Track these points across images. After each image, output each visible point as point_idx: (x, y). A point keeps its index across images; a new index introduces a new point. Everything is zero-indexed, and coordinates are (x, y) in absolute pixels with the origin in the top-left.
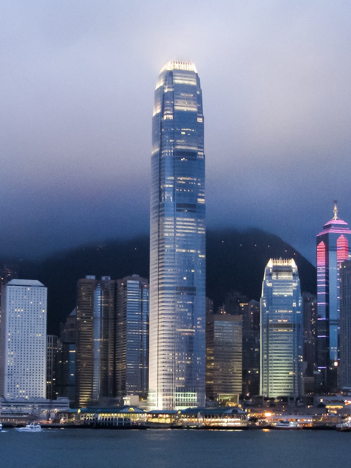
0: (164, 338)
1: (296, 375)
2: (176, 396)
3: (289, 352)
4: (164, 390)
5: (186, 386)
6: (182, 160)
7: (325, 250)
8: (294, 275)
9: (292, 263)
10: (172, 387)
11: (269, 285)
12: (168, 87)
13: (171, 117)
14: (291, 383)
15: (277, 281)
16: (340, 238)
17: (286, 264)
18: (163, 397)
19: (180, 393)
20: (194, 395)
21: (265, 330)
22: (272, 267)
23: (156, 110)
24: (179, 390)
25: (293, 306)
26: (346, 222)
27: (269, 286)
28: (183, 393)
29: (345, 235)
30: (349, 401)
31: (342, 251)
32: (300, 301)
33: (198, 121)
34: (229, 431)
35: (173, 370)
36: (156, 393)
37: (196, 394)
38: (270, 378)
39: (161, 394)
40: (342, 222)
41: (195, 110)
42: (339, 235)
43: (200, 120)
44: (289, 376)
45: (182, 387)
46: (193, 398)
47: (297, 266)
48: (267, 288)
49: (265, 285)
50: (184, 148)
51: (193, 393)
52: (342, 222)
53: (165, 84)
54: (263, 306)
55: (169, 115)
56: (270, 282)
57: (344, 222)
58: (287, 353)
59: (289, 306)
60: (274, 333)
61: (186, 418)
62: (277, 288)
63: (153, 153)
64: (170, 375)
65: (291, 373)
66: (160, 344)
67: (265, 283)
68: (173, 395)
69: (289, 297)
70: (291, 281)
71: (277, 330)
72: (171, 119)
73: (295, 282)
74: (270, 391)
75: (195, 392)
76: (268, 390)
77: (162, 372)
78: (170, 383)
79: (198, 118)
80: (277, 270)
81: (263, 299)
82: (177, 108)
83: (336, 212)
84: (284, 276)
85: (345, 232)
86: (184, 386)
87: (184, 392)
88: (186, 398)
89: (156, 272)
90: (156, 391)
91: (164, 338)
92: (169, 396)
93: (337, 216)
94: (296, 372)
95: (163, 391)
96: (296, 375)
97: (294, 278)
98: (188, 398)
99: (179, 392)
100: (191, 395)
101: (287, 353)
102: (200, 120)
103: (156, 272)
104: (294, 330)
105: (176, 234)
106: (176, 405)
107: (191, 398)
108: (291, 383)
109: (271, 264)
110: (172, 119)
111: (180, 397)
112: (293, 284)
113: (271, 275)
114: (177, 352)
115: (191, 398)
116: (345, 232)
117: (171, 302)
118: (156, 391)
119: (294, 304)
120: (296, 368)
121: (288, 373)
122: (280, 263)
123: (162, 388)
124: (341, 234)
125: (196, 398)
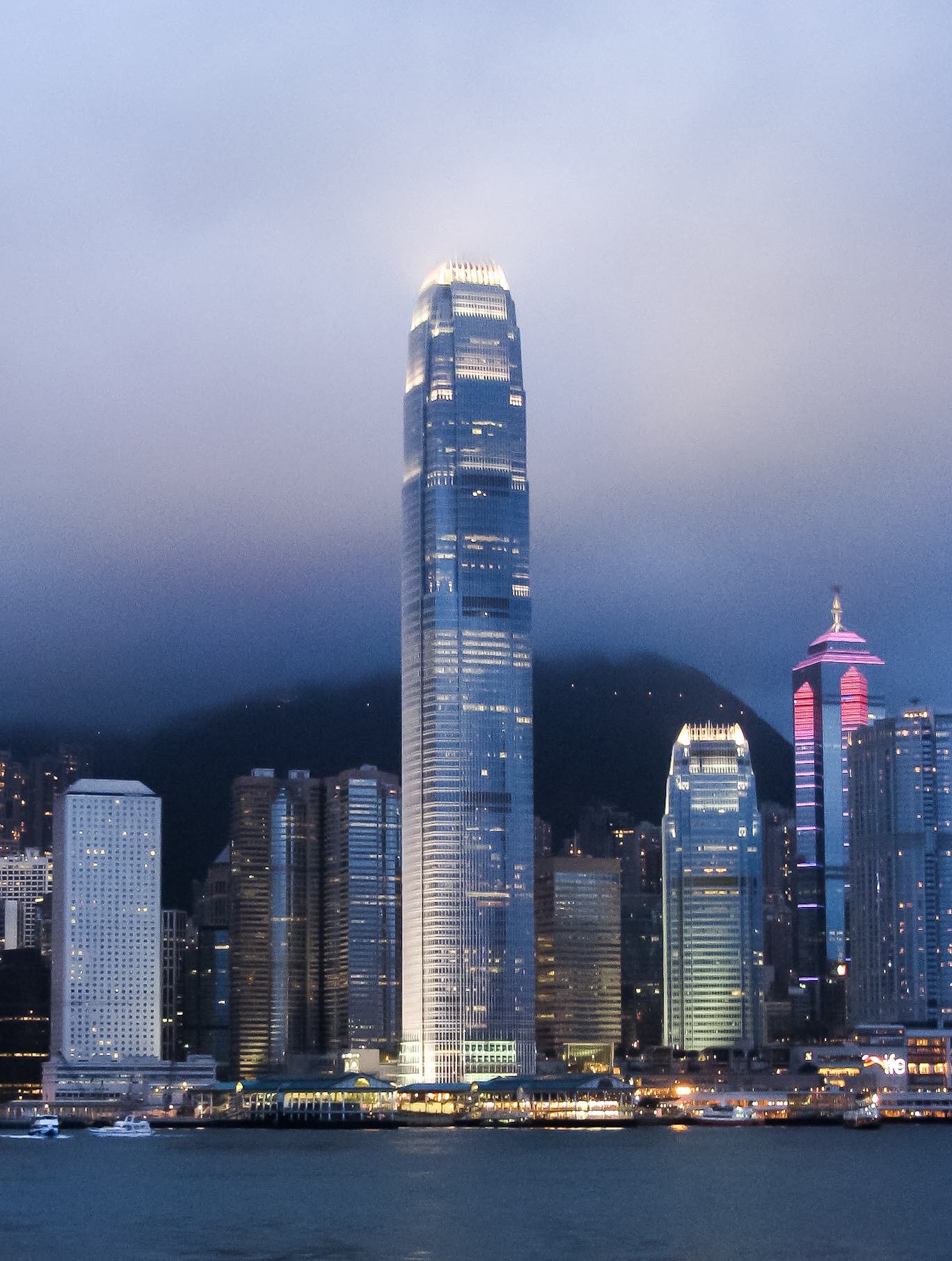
0: (436, 914)
1: (748, 998)
4: (438, 1037)
8: (740, 762)
10: (456, 1029)
13: (447, 394)
14: (735, 1016)
15: (701, 776)
17: (721, 737)
18: (437, 1052)
19: (477, 1043)
21: (674, 893)
23: (412, 379)
24: (473, 1035)
26: (860, 636)
28: (483, 1043)
30: (872, 1058)
31: (852, 704)
32: (755, 823)
35: (458, 990)
36: (419, 1044)
39: (430, 1044)
40: (851, 637)
41: (503, 376)
43: (517, 399)
46: (507, 1053)
47: (747, 742)
49: (674, 788)
51: (507, 1043)
52: (851, 637)
53: (434, 317)
54: (669, 835)
56: (684, 780)
57: (856, 636)
61: (491, 1100)
62: (702, 794)
65: (736, 993)
66: (427, 929)
67: (673, 781)
68: (458, 1046)
69: (730, 814)
70: (734, 778)
73: (743, 779)
74: (686, 1035)
75: (510, 1039)
80: (702, 751)
81: (669, 819)
82: (461, 373)
84: (719, 766)
85: (859, 660)
86: (484, 1026)
87: (486, 1039)
88: (489, 1054)
90: (419, 1038)
93: (841, 622)
94: (748, 989)
96: (748, 998)
97: (741, 770)
98: (495, 1053)
100: (501, 1048)
101: (726, 946)
102: (515, 401)
104: (742, 892)
107: (501, 1054)
108: (735, 1016)
109: (685, 737)
112: (739, 783)
113: (686, 762)
115: (501, 1054)
116: (859, 660)
117: (453, 829)
118: (420, 1038)
119: (742, 831)
120: (747, 982)
122: (708, 734)
123: (434, 1030)
124: (849, 665)
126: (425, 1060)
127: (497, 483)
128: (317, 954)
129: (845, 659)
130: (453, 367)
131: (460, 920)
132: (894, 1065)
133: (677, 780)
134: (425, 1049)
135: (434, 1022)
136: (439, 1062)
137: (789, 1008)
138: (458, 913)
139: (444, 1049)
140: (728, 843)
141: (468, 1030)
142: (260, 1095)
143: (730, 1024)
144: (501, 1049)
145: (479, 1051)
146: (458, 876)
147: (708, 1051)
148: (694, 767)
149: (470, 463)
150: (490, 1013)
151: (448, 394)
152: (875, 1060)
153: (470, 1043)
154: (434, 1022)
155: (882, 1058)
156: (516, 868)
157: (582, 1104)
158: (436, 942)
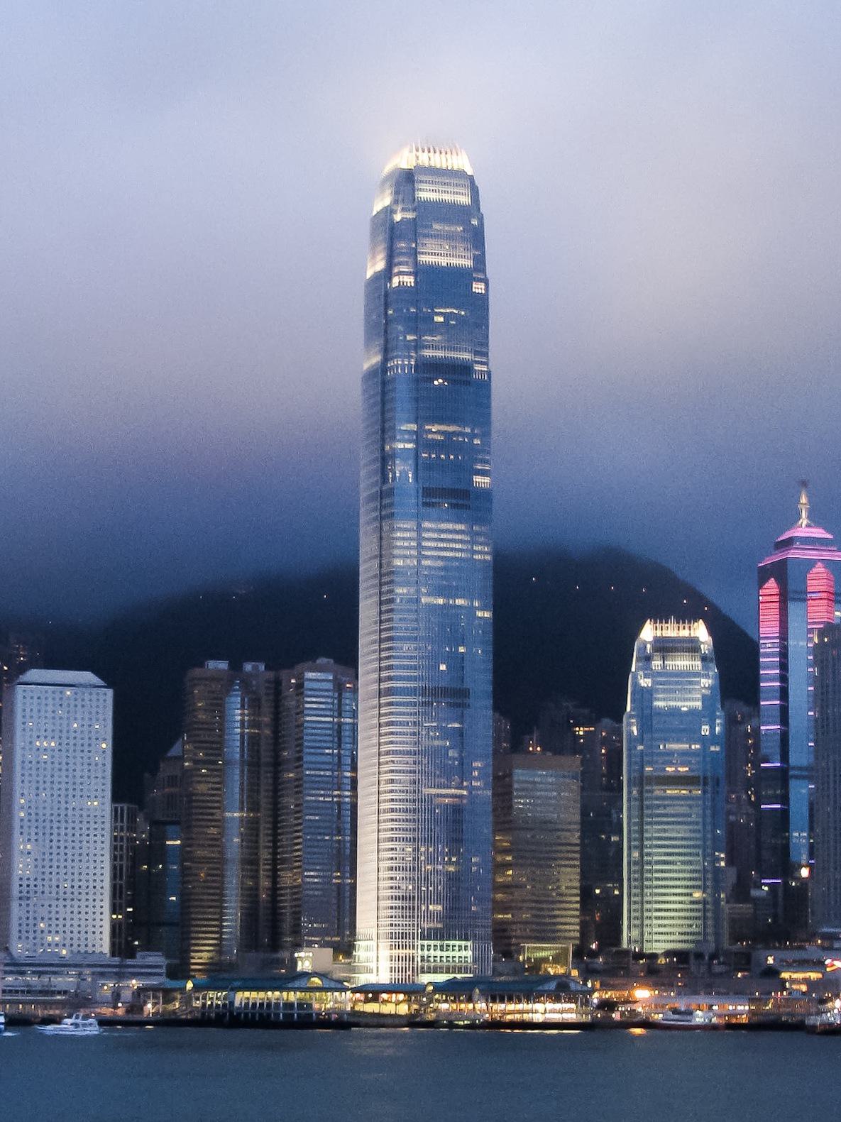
0: (392, 810)
1: (709, 899)
2: (422, 950)
3: (691, 843)
4: (392, 936)
5: (446, 926)
6: (436, 383)
7: (778, 600)
8: (704, 659)
9: (700, 631)
11: (645, 682)
12: (403, 210)
13: (409, 280)
14: (696, 918)
15: (664, 673)
16: (814, 570)
17: (684, 633)
18: (392, 951)
19: (432, 943)
20: (466, 948)
21: (635, 792)
22: (651, 639)
23: (374, 265)
24: (429, 935)
25: (703, 734)
26: (828, 531)
27: (646, 686)
28: (438, 943)
29: (827, 563)
30: (835, 963)
31: (819, 601)
32: (718, 721)
33: (474, 290)
34: (550, 1034)
35: (414, 888)
36: (374, 943)
37: (469, 943)
38: (646, 906)
39: (385, 944)
40: (818, 533)
42: (811, 563)
44: (692, 903)
45: (436, 929)
46: (463, 953)
47: (710, 638)
48: (639, 691)
50: (441, 355)
51: (463, 943)
52: (818, 533)
53: (396, 202)
54: (630, 733)
55: (405, 277)
56: (646, 676)
57: (823, 531)
58: (688, 847)
59: (693, 735)
60: (657, 798)
61: (446, 1001)
63: (366, 366)
64: (406, 900)
65: (697, 895)
66: (383, 826)
68: (413, 946)
69: (692, 712)
70: (698, 675)
71: (665, 790)
72: (409, 285)
73: (707, 676)
74: (646, 937)
75: (466, 939)
76: (642, 934)
77: (389, 893)
78: (408, 919)
79: (474, 283)
80: (665, 647)
81: (631, 716)
82: (423, 259)
83: (806, 508)
84: (682, 663)
86: (440, 925)
87: (442, 939)
88: (445, 954)
89: (374, 651)
90: (373, 937)
91: (392, 810)
92: (406, 949)
93: (808, 517)
94: (709, 891)
95: (392, 938)
96: (709, 899)
98: (451, 954)
99: (429, 939)
100: (457, 948)
101: (688, 847)
102: (478, 288)
103: (374, 651)
104: (704, 792)
105: (423, 562)
106: (423, 972)
107: (457, 954)
108: (696, 918)
109: (648, 633)
110: (413, 285)
111: (432, 953)
113: (648, 659)
114: (425, 845)
115: (457, 954)
116: (827, 556)
117: (410, 724)
118: (375, 937)
119: (705, 730)
120: (709, 883)
121: (691, 895)
122: (671, 630)
123: (389, 930)
124: (816, 561)
125: (470, 953)
127: (463, 370)
130: (415, 253)
145: (434, 951)
147: (668, 954)
148: (656, 664)
153: (426, 943)
157: (539, 1007)
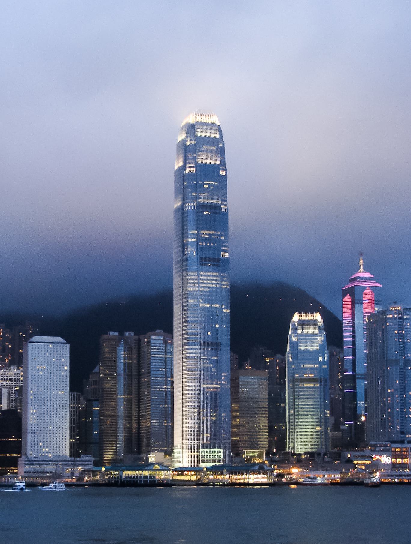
0: (188, 394)
1: (323, 430)
2: (202, 453)
4: (189, 447)
6: (205, 213)
8: (320, 329)
9: (318, 317)
10: (197, 444)
11: (295, 339)
13: (193, 170)
14: (317, 438)
16: (366, 291)
17: (311, 318)
18: (189, 454)
19: (206, 450)
21: (291, 385)
23: (178, 164)
24: (204, 447)
25: (320, 360)
26: (371, 274)
27: (295, 340)
28: (208, 450)
30: (376, 456)
32: (326, 355)
35: (198, 427)
36: (181, 450)
39: (186, 451)
40: (368, 275)
43: (223, 172)
46: (219, 454)
47: (322, 320)
49: (291, 340)
50: (207, 201)
51: (219, 450)
52: (368, 275)
54: (289, 360)
56: (295, 336)
57: (369, 274)
59: (315, 361)
62: (303, 342)
65: (318, 428)
66: (184, 401)
67: (291, 337)
68: (198, 451)
69: (315, 351)
70: (317, 335)
73: (321, 336)
75: (220, 448)
80: (303, 324)
81: (289, 353)
82: (199, 161)
84: (310, 330)
85: (371, 285)
86: (209, 443)
87: (210, 448)
88: (211, 455)
90: (181, 448)
93: (363, 268)
94: (323, 427)
96: (323, 430)
98: (214, 454)
100: (216, 452)
104: (320, 385)
107: (216, 455)
108: (317, 438)
109: (296, 318)
111: (206, 454)
112: (319, 338)
113: (296, 329)
115: (216, 455)
116: (371, 285)
117: (195, 358)
118: (181, 448)
119: (321, 359)
120: (323, 424)
122: (306, 317)
123: (187, 444)
124: (367, 287)
126: (183, 457)
128: (137, 411)
129: (365, 284)
130: (195, 158)
131: (198, 397)
132: (386, 459)
133: (292, 337)
134: (184, 453)
135: (187, 441)
136: (189, 458)
137: (341, 435)
138: (198, 394)
139: (192, 452)
140: (314, 364)
141: (202, 444)
142: (112, 473)
143: (315, 442)
144: (216, 453)
146: (198, 378)
149: (203, 200)
150: (212, 437)
151: (193, 170)
152: (378, 457)
153: (203, 450)
154: (187, 441)
155: (381, 456)
156: (223, 374)
158: (188, 406)
